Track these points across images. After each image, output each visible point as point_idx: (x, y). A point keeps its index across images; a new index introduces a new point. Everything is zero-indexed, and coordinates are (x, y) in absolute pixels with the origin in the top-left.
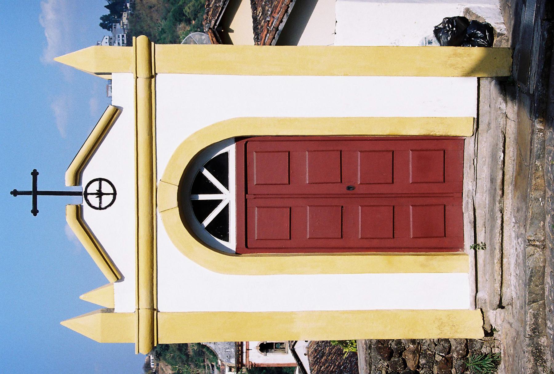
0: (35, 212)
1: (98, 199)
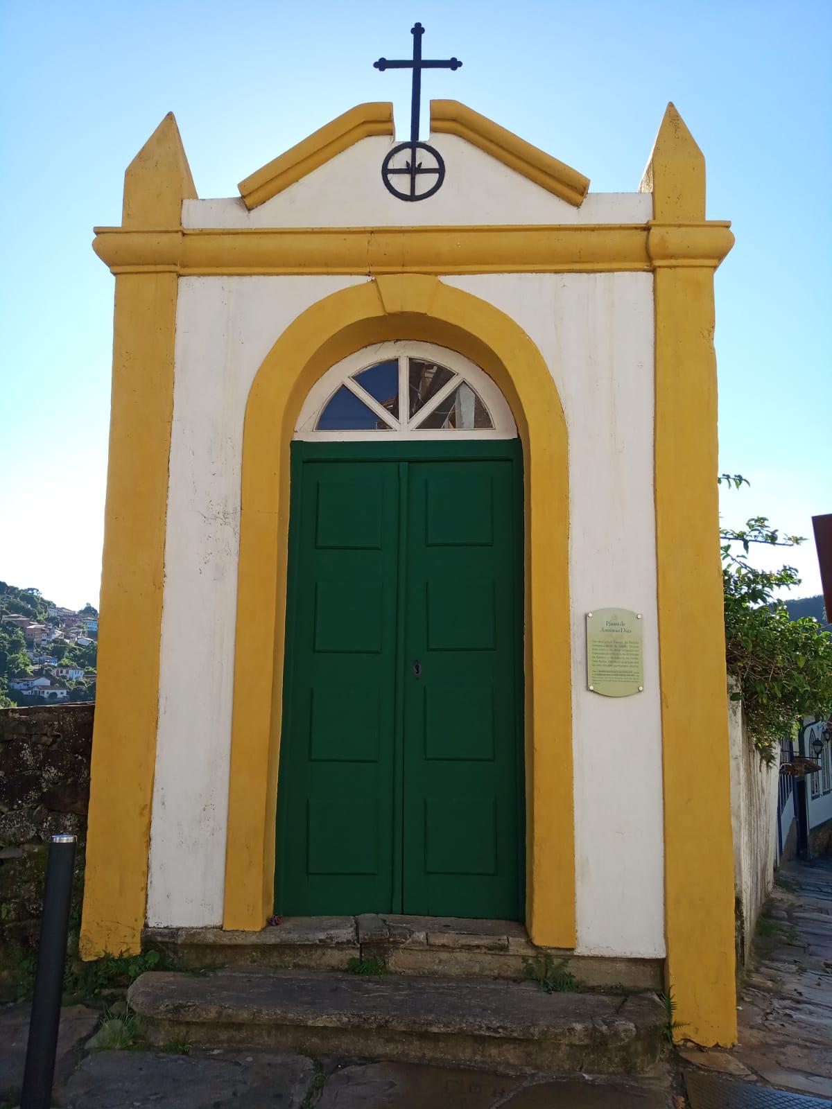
0: (382, 65)
1: (404, 167)
